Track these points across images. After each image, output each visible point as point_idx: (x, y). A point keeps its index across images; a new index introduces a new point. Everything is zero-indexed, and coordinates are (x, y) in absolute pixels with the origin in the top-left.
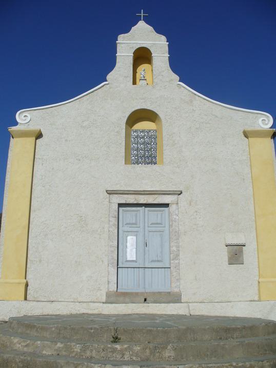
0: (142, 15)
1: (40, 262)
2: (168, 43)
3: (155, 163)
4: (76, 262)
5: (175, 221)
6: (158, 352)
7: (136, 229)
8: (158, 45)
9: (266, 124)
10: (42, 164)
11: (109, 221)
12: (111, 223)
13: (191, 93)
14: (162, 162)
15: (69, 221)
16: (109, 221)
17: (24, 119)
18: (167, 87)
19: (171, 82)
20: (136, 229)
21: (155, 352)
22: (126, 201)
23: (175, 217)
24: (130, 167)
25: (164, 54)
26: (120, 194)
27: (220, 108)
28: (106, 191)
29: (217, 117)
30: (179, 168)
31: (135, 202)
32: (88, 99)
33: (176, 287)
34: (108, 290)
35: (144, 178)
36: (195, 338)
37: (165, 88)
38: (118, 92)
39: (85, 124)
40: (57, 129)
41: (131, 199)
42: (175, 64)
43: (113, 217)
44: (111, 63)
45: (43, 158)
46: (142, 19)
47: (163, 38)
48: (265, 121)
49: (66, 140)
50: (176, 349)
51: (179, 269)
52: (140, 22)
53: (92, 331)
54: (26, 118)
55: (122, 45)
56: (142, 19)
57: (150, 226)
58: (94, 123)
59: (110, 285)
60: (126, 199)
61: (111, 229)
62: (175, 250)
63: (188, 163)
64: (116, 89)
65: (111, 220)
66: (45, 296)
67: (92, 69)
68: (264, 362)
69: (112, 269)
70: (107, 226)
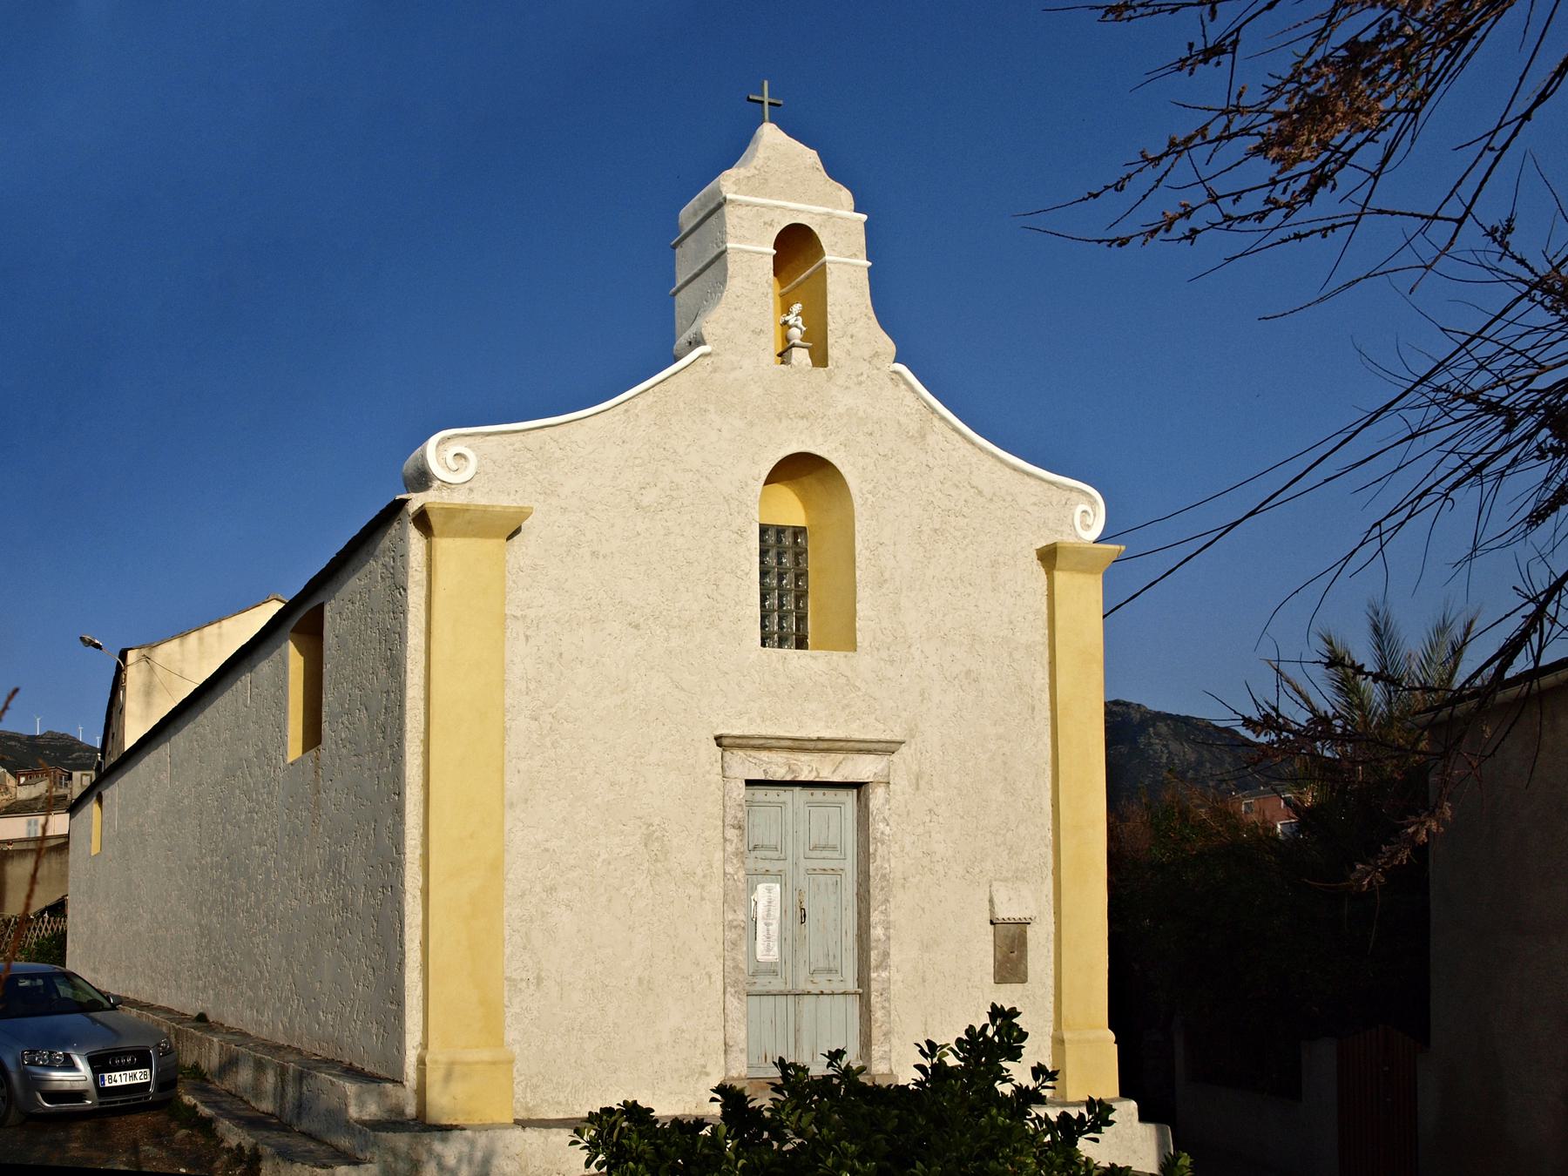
1: (538, 984)
2: (864, 217)
3: (763, 645)
4: (640, 980)
7: (779, 866)
8: (838, 220)
10: (527, 638)
11: (725, 840)
12: (730, 848)
13: (916, 405)
14: (847, 641)
15: (617, 840)
16: (725, 840)
17: (452, 464)
18: (863, 378)
19: (875, 361)
20: (779, 866)
22: (765, 772)
23: (882, 826)
24: (773, 653)
25: (855, 256)
26: (754, 747)
27: (990, 462)
28: (717, 738)
29: (980, 493)
31: (788, 778)
32: (650, 407)
34: (727, 1070)
37: (860, 383)
39: (649, 498)
40: (564, 510)
41: (777, 766)
45: (524, 617)
48: (1084, 515)
51: (888, 1000)
54: (458, 462)
55: (743, 211)
58: (674, 494)
60: (765, 766)
61: (730, 870)
63: (913, 649)
66: (559, 1103)
70: (719, 855)
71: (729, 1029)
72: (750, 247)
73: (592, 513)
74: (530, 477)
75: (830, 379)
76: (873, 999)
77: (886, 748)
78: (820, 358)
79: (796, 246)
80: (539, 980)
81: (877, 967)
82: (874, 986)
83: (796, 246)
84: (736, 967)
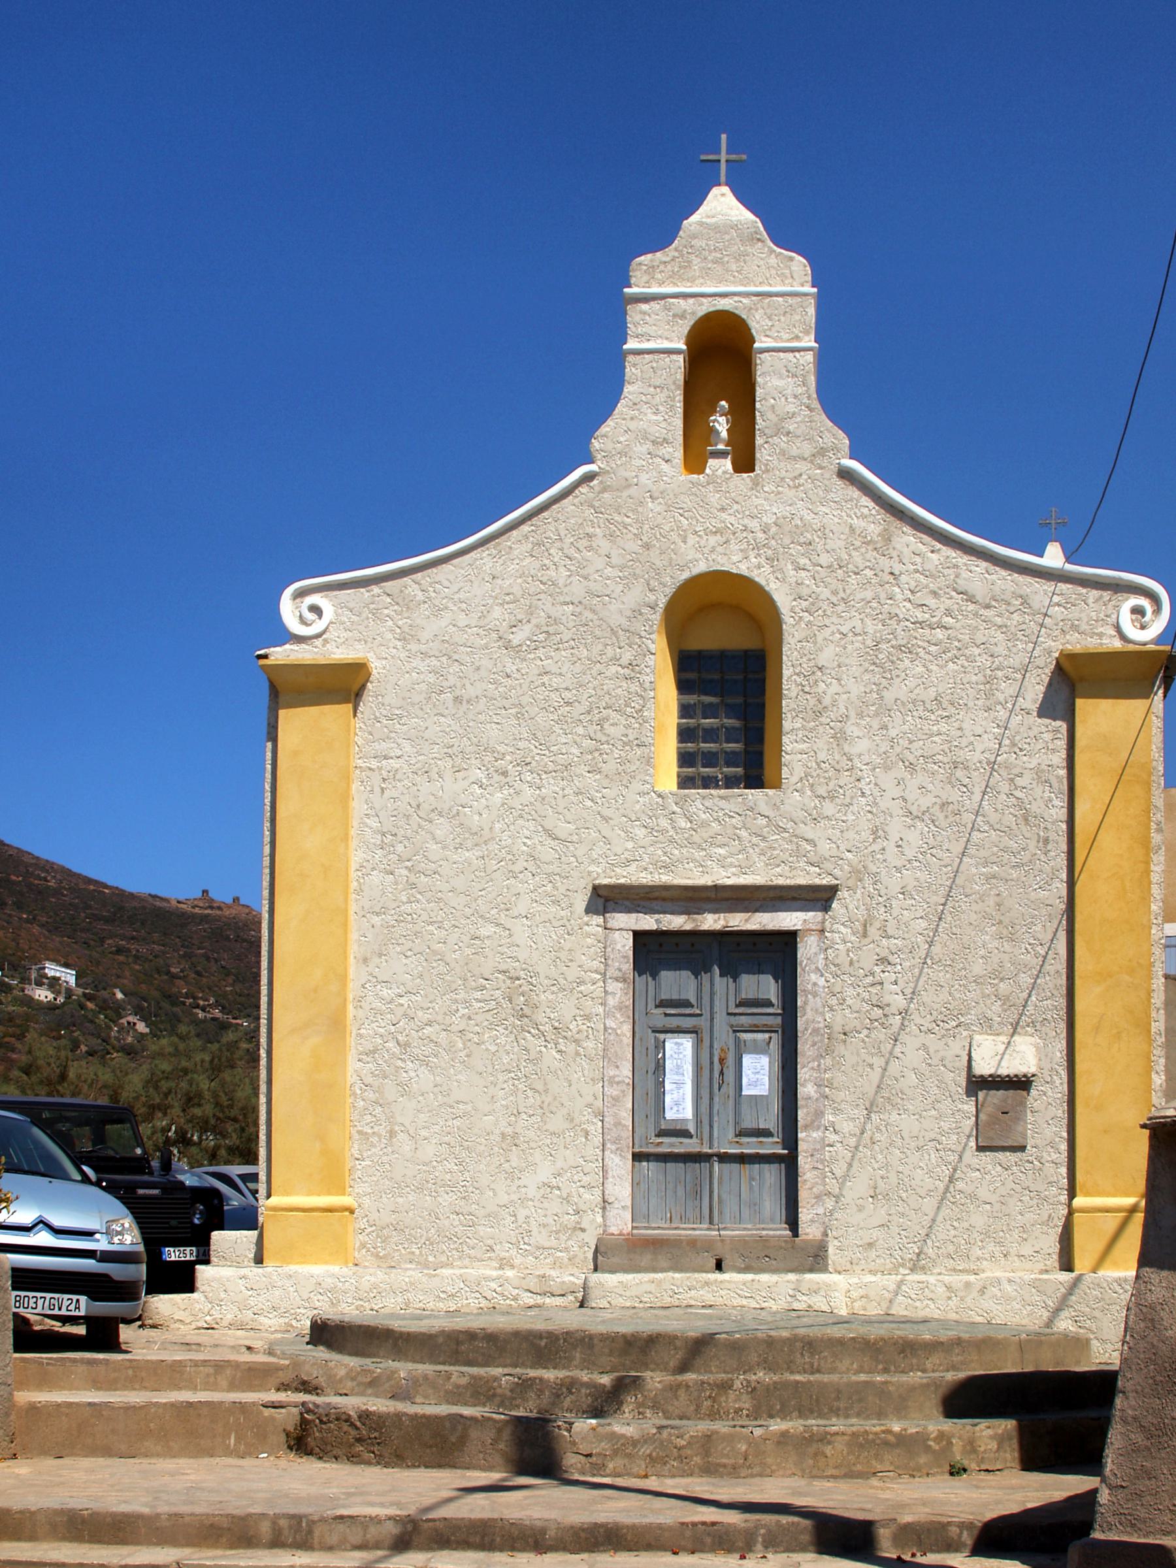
0: (723, 157)
2: (815, 290)
5: (815, 995)
6: (710, 1397)
7: (688, 1023)
9: (1143, 627)
10: (383, 790)
11: (606, 992)
12: (612, 1001)
14: (777, 785)
15: (478, 995)
16: (606, 992)
20: (688, 1023)
21: (699, 1397)
23: (813, 977)
30: (832, 798)
33: (812, 1221)
35: (722, 843)
36: (816, 1365)
38: (643, 506)
42: (838, 391)
43: (617, 979)
44: (599, 384)
45: (380, 769)
46: (723, 178)
47: (799, 264)
49: (457, 700)
50: (754, 1389)
52: (715, 191)
53: (543, 1343)
54: (318, 620)
56: (723, 178)
57: (733, 1010)
58: (551, 630)
59: (612, 1213)
61: (610, 1023)
62: (813, 1094)
64: (625, 494)
65: (610, 989)
67: (510, 438)
68: (977, 1428)
69: (617, 1159)
71: (609, 1186)
72: (656, 338)
73: (456, 657)
74: (390, 623)
75: (756, 484)
76: (801, 1160)
77: (820, 898)
78: (745, 462)
79: (720, 358)
80: (392, 1134)
81: (806, 1127)
82: (802, 1146)
83: (720, 358)
84: (618, 1124)
